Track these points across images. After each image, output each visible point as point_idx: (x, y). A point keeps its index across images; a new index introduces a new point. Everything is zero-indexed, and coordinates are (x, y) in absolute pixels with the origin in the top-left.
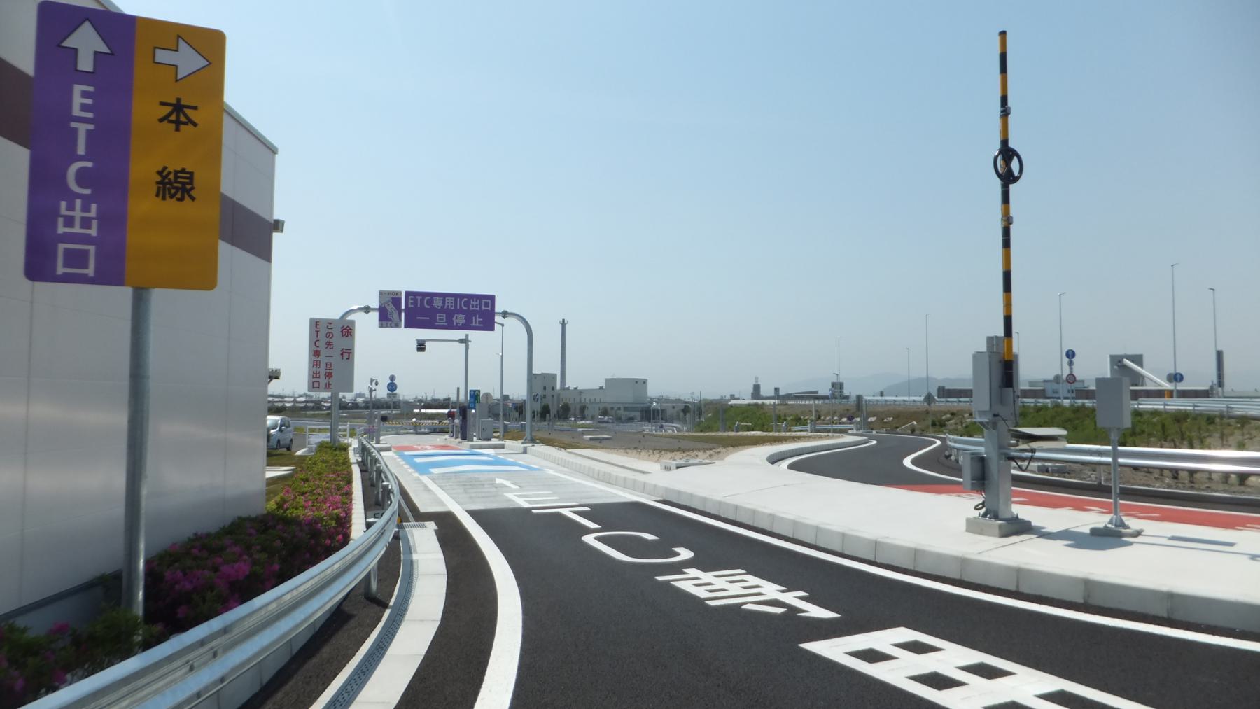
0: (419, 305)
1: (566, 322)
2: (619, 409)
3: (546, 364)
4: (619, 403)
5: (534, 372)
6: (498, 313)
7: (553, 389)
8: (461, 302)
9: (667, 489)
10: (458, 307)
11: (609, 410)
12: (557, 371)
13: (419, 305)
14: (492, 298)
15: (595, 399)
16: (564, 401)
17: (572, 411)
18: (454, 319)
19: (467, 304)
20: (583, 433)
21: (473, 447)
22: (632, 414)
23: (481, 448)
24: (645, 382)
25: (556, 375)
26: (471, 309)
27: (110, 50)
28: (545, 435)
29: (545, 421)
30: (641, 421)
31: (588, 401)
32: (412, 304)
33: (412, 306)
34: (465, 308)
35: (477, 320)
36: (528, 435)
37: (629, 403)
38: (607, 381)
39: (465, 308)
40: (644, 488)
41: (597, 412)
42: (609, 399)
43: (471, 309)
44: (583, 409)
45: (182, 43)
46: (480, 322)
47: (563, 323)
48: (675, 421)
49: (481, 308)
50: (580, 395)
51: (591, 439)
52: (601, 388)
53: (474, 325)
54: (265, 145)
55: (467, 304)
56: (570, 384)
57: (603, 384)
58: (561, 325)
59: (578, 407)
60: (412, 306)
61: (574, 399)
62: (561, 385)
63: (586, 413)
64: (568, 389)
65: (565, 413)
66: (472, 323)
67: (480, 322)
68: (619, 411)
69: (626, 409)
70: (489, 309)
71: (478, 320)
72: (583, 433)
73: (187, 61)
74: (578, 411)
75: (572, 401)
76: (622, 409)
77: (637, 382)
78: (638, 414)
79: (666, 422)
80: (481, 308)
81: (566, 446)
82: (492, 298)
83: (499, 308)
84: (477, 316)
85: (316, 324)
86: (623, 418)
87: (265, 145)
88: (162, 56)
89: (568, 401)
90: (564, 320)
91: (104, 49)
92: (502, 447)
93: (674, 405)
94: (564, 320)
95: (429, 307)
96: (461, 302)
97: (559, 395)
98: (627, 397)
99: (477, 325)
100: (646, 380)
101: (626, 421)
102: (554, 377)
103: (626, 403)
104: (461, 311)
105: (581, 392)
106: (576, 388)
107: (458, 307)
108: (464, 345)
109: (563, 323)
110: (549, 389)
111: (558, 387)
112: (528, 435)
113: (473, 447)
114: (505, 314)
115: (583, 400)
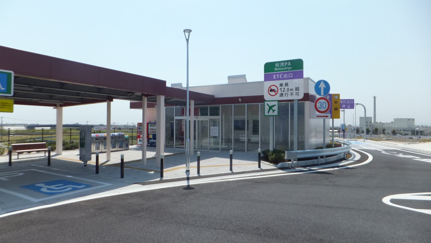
0: (278, 78)
1: (376, 97)
2: (401, 130)
3: (370, 114)
4: (400, 128)
5: (141, 152)
6: (355, 104)
7: (370, 122)
8: (344, 101)
9: (403, 147)
10: (343, 103)
11: (396, 131)
12: (373, 116)
13: (278, 78)
14: (353, 100)
15: (389, 126)
16: (375, 127)
17: (379, 131)
18: (342, 106)
19: (346, 102)
20: (383, 137)
21: (348, 140)
22: (407, 133)
23: (350, 140)
24: (413, 120)
25: (148, 107)
26: (347, 103)
27: (330, 97)
28: (370, 138)
29: (369, 134)
30: (411, 135)
31: (386, 127)
32: (275, 77)
33: (275, 78)
34: (345, 103)
35: (349, 106)
36: (365, 137)
37: (406, 128)
38: (395, 119)
39: (345, 103)
40: (398, 147)
41: (390, 132)
42: (396, 126)
43: (347, 103)
44: (384, 130)
45: (336, 96)
46: (350, 107)
47: (375, 98)
48: (428, 136)
49: (350, 103)
50: (383, 125)
51: (386, 139)
52: (392, 122)
53: (348, 107)
54: (313, 81)
55: (346, 102)
56: (378, 120)
57: (393, 121)
58: (373, 99)
59: (382, 129)
60: (275, 78)
61: (380, 126)
62: (374, 121)
63: (385, 132)
64: (377, 122)
65: (376, 132)
66: (347, 107)
67: (350, 107)
68: (400, 131)
69: (404, 130)
70: (353, 103)
71: (349, 106)
72: (383, 137)
73: (336, 97)
74: (382, 131)
75: (379, 127)
76: (402, 130)
77: (409, 120)
78: (410, 133)
79: (424, 136)
80: (350, 103)
81: (377, 140)
82: (353, 100)
83: (355, 102)
84: (349, 105)
85: (360, 117)
86: (403, 134)
87: (313, 81)
88: (334, 97)
89: (377, 127)
90: (375, 97)
91: (329, 97)
92: (357, 140)
93: (426, 129)
94: (375, 97)
95: (282, 78)
96: (344, 101)
97: (373, 125)
98: (405, 126)
99: (349, 107)
100: (414, 119)
101: (404, 135)
102: (371, 118)
103: (404, 128)
104: (344, 104)
105: (383, 124)
106: (380, 122)
107: (343, 103)
108: (343, 112)
109: (375, 98)
110: (369, 122)
111: (373, 122)
112: (365, 137)
113: (348, 140)
114: (357, 104)
115: (384, 127)
